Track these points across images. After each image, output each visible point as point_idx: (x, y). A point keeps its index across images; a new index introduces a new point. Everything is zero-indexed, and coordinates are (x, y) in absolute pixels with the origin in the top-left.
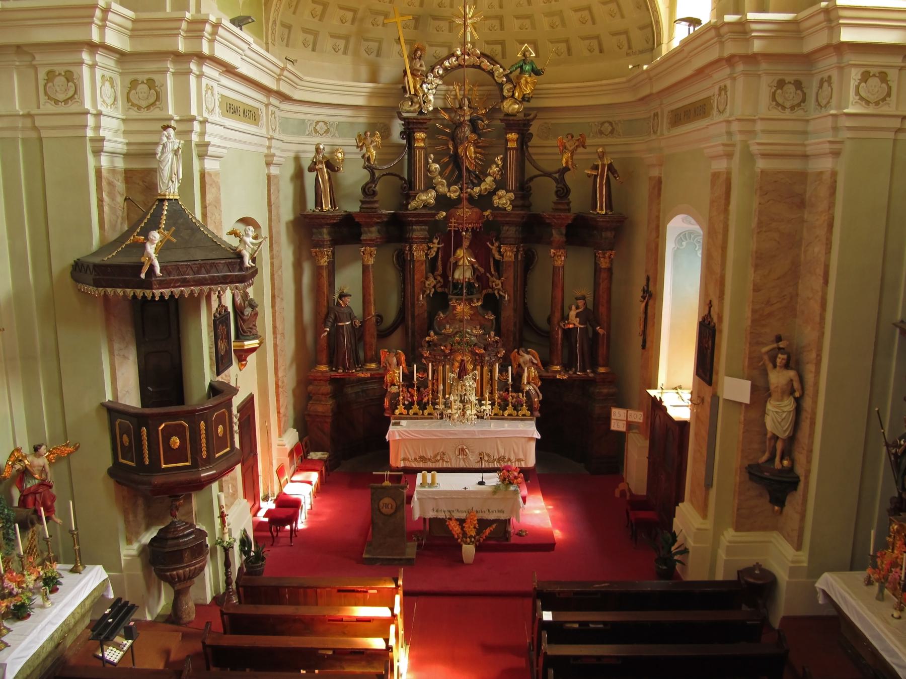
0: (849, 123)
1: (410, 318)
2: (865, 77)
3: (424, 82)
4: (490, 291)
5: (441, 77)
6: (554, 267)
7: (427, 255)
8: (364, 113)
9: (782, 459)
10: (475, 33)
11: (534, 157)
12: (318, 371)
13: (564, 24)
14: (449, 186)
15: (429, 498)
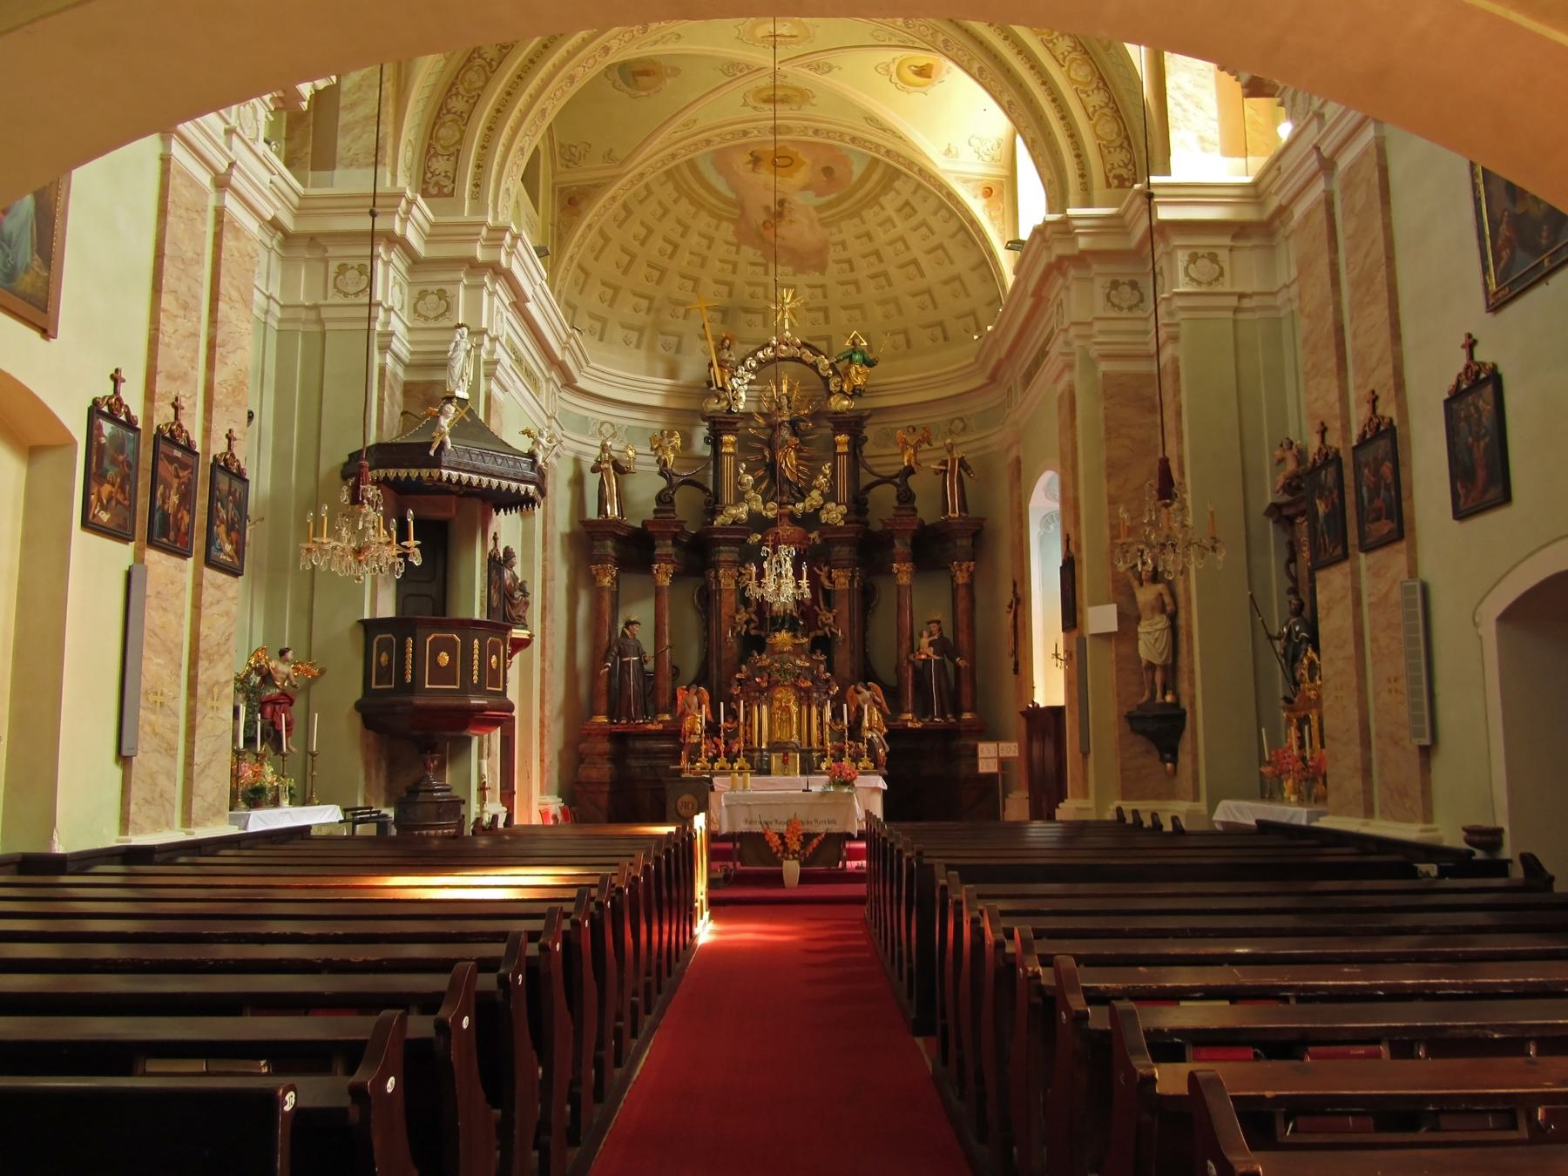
0: (1179, 302)
1: (715, 663)
2: (1194, 258)
3: (733, 376)
4: (820, 633)
5: (754, 371)
6: (899, 586)
8: (659, 418)
9: (1164, 694)
10: (794, 320)
11: (869, 462)
12: (593, 723)
13: (900, 312)
14: (765, 503)
15: (740, 804)
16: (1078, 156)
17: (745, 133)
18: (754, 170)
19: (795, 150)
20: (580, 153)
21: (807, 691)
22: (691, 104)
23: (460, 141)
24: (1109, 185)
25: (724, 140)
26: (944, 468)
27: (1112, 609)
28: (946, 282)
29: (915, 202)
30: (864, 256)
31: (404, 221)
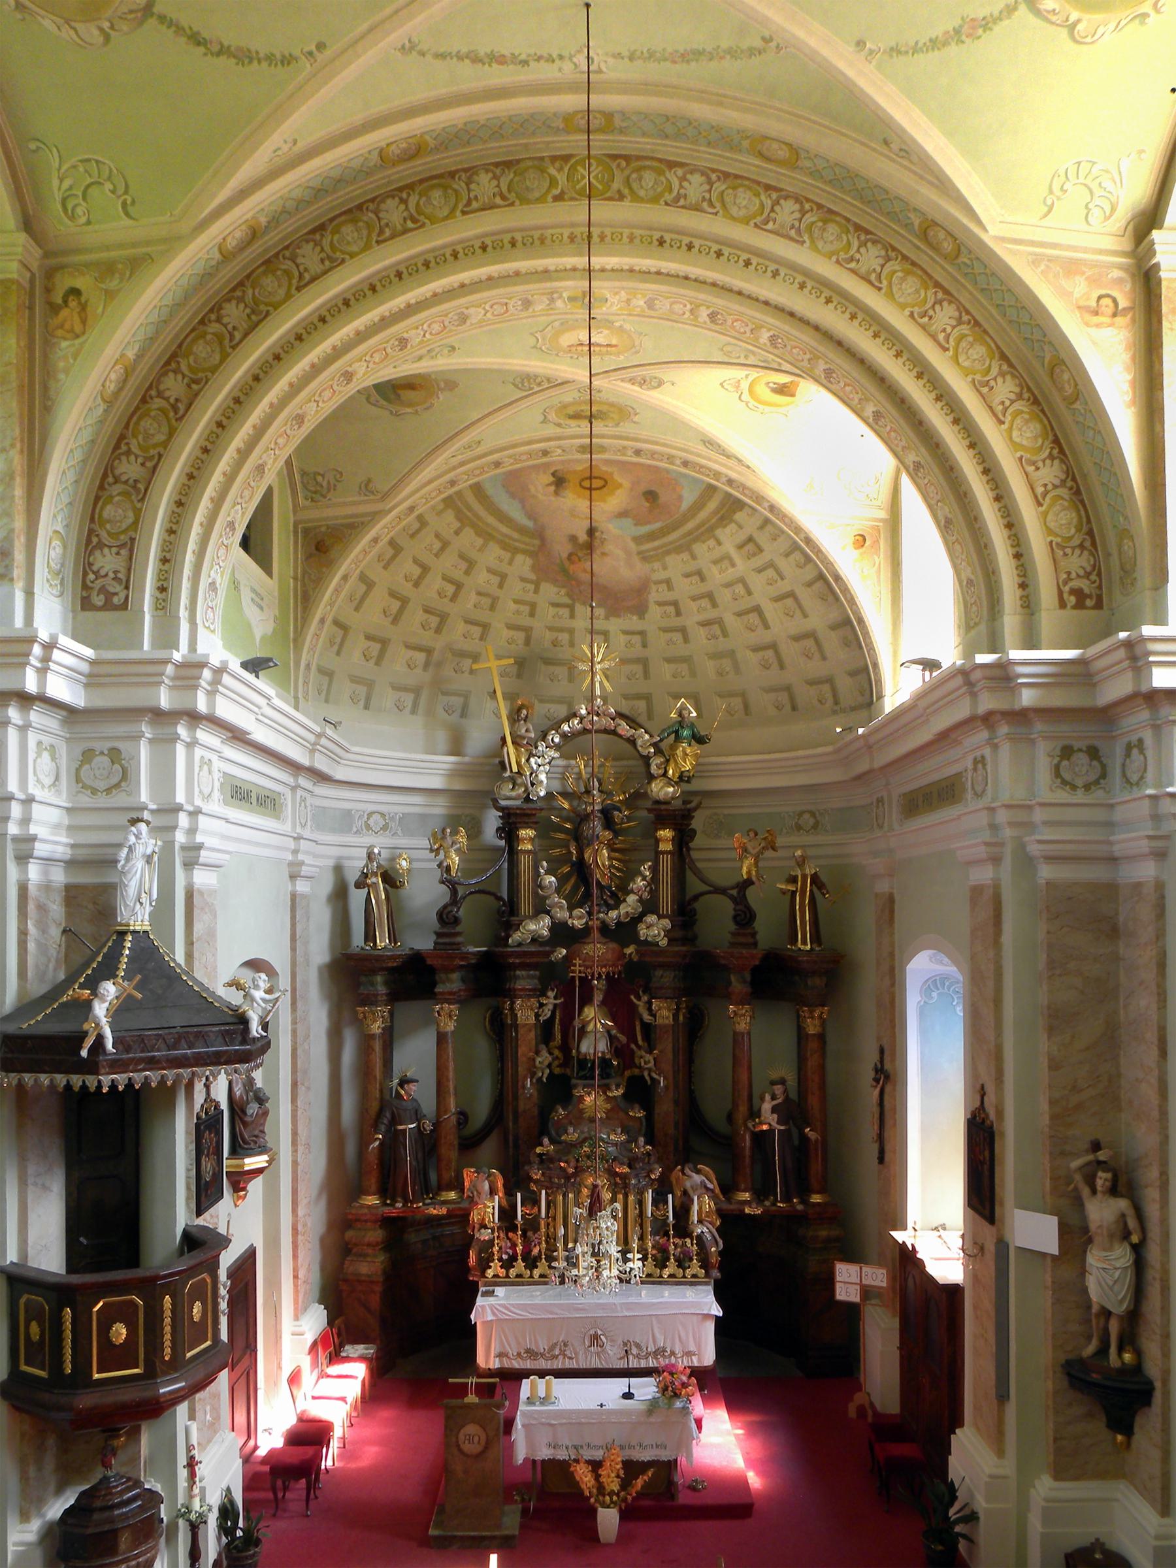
3: (531, 755)
5: (557, 747)
6: (735, 1033)
7: (537, 1016)
9: (1121, 1349)
10: (607, 684)
11: (699, 865)
12: (362, 1206)
14: (571, 908)
15: (543, 1424)
16: (1018, 556)
17: (545, 453)
18: (556, 493)
19: (610, 470)
20: (329, 482)
21: (624, 1177)
22: (473, 424)
23: (135, 524)
24: (1062, 604)
25: (516, 461)
26: (791, 888)
27: (1050, 1224)
28: (797, 638)
29: (762, 539)
30: (694, 599)
31: (43, 671)
